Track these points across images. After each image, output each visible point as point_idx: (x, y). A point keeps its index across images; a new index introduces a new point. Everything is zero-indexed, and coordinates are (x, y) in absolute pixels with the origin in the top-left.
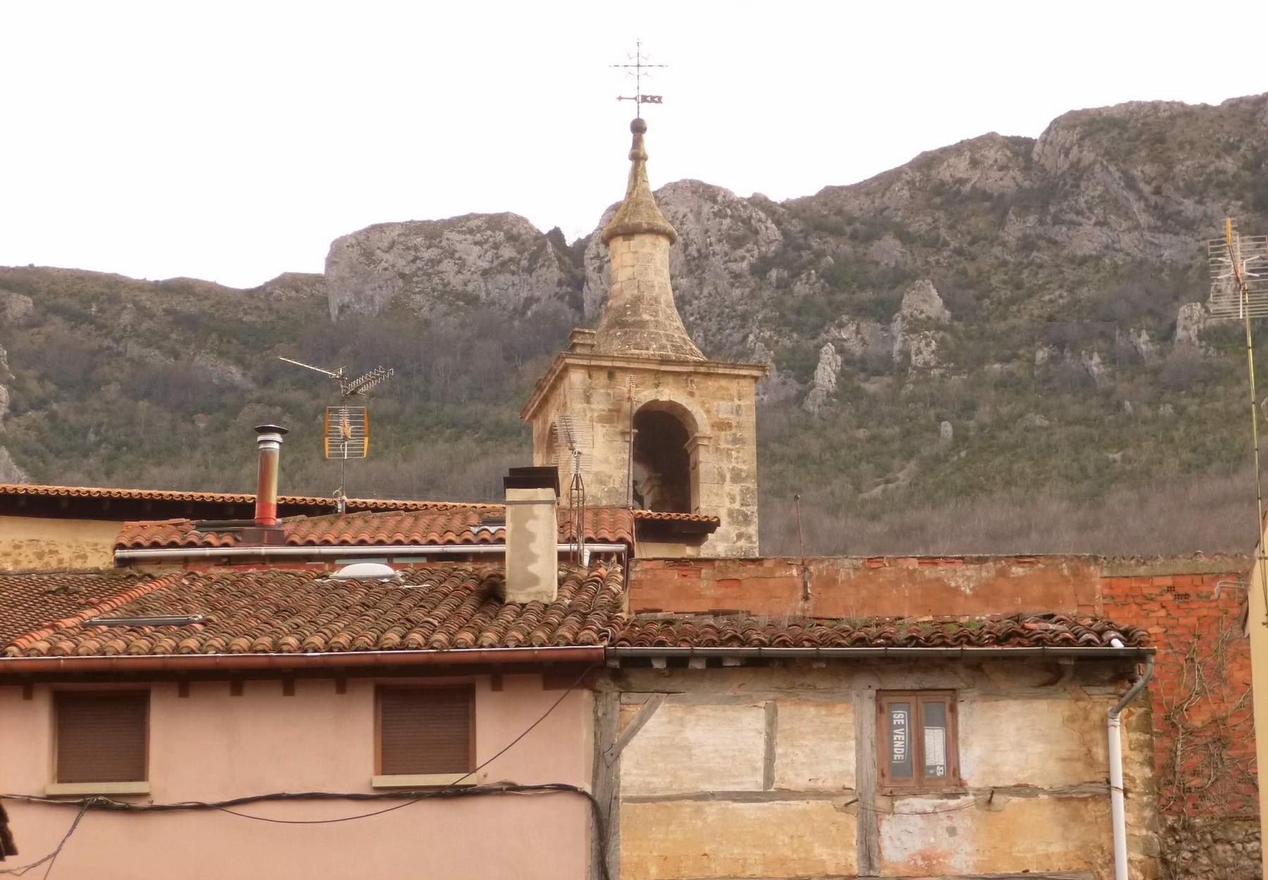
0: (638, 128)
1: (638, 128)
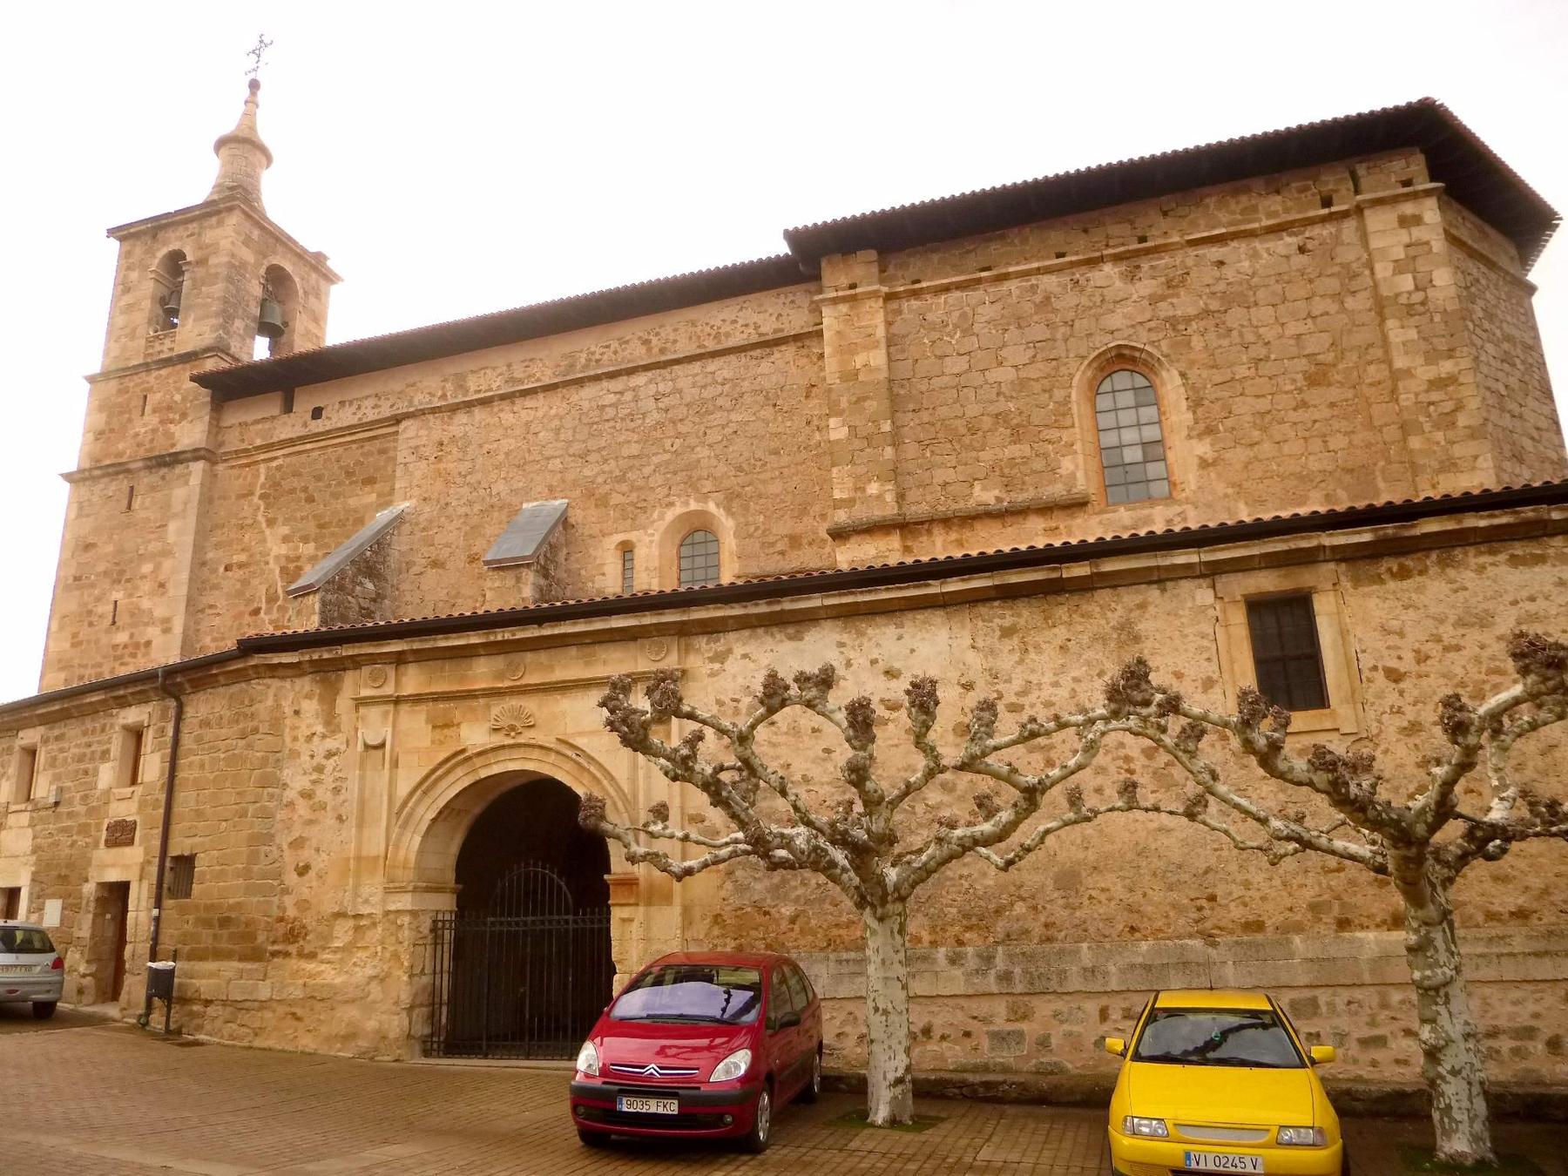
0: (254, 85)
1: (254, 85)
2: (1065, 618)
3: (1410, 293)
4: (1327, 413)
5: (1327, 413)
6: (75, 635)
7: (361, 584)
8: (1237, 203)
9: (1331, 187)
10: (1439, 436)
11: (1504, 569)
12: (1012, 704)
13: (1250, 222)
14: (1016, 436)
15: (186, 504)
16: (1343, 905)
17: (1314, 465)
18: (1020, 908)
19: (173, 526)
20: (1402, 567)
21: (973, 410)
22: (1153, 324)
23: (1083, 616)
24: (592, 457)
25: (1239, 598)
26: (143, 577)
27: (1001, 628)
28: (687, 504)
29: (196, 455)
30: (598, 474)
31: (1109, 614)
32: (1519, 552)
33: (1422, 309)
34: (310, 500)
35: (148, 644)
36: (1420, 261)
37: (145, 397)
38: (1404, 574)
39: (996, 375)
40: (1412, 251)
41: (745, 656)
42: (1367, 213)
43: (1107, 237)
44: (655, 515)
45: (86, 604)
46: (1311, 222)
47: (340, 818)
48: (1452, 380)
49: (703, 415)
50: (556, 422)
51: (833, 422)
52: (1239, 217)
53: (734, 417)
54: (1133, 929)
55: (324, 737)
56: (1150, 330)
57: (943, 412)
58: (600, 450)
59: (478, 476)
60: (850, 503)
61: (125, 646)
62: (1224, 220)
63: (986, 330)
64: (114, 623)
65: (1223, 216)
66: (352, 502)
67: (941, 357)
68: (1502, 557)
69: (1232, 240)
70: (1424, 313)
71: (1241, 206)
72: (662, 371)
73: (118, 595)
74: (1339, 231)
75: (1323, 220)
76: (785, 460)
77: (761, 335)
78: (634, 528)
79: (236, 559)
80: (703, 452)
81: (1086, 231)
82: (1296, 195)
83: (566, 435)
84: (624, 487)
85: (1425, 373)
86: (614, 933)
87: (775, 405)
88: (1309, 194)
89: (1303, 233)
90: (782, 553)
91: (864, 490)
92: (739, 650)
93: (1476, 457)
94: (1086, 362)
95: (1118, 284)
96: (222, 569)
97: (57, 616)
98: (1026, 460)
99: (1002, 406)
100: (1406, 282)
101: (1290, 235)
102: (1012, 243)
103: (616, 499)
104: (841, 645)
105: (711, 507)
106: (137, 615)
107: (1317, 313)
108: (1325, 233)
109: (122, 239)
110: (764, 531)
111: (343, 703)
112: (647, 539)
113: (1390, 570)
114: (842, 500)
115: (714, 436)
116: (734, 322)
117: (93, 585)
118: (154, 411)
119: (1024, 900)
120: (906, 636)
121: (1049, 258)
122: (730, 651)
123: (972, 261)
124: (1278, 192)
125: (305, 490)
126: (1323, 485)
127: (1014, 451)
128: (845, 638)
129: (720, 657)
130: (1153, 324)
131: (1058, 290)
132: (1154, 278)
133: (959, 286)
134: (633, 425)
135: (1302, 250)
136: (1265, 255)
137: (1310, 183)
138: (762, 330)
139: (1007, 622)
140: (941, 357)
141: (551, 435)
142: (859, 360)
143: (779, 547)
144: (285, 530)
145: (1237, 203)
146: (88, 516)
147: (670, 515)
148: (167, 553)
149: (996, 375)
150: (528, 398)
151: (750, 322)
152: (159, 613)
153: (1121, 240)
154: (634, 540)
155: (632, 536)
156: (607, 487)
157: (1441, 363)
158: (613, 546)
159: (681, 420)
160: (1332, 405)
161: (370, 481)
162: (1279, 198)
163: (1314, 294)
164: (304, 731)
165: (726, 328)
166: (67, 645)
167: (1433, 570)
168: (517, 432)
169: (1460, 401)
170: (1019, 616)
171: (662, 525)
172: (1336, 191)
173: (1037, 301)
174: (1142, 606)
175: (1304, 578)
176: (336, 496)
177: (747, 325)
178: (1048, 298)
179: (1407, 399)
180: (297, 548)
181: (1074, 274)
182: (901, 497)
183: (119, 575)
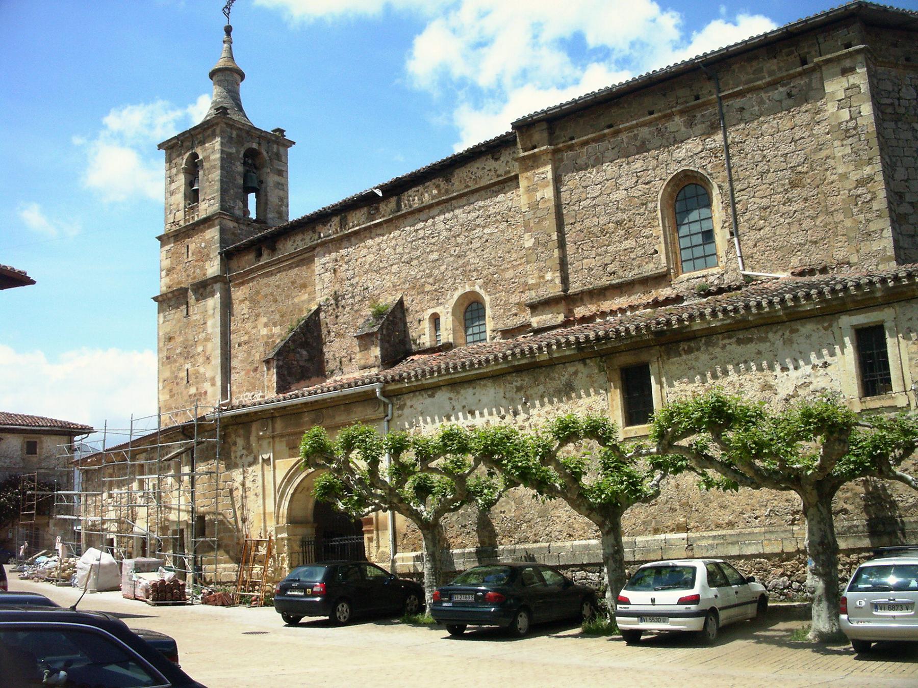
0: (228, 30)
2: (543, 380)
3: (847, 122)
4: (801, 205)
5: (801, 205)
6: (171, 391)
7: (299, 353)
8: (751, 66)
9: (806, 50)
10: (861, 217)
11: (734, 346)
12: (521, 426)
13: (759, 79)
14: (627, 235)
15: (214, 309)
16: (656, 522)
17: (794, 241)
18: (524, 526)
19: (209, 323)
20: (689, 347)
21: (603, 220)
22: (703, 154)
23: (550, 379)
24: (415, 262)
25: (616, 367)
26: (199, 354)
27: (516, 387)
28: (464, 287)
29: (215, 279)
30: (417, 272)
31: (562, 377)
32: (741, 337)
33: (854, 132)
34: (275, 301)
35: (206, 393)
36: (853, 99)
37: (188, 246)
38: (689, 351)
39: (616, 196)
40: (849, 93)
41: (411, 406)
42: (823, 68)
43: (677, 98)
44: (448, 297)
45: (174, 372)
46: (794, 77)
47: (256, 494)
48: (870, 179)
49: (470, 231)
50: (394, 242)
51: (527, 236)
52: (752, 76)
53: (486, 231)
54: (570, 536)
55: (247, 456)
56: (702, 158)
57: (587, 223)
58: (418, 258)
59: (357, 279)
60: (536, 286)
61: (195, 395)
62: (743, 79)
63: (610, 167)
64: (188, 382)
65: (743, 77)
66: (296, 300)
67: (586, 187)
68: (733, 340)
69: (748, 93)
70: (855, 135)
71: (754, 68)
72: (446, 204)
73: (188, 366)
74: (811, 81)
75: (800, 74)
76: (514, 256)
77: (498, 176)
78: (439, 304)
79: (243, 339)
80: (471, 255)
81: (664, 95)
82: (785, 58)
83: (399, 249)
84: (431, 280)
85: (854, 176)
86: (366, 544)
87: (507, 221)
88: (793, 56)
89: (789, 83)
90: (516, 315)
91: (543, 277)
92: (409, 403)
93: (882, 230)
94: (666, 183)
95: (683, 129)
96: (237, 346)
97: (161, 380)
98: (632, 250)
99: (620, 216)
100: (845, 114)
101: (782, 86)
102: (624, 108)
103: (428, 288)
104: (450, 399)
105: (477, 289)
106: (198, 376)
107: (797, 138)
108: (802, 82)
109: (166, 149)
110: (505, 301)
111: (253, 439)
112: (445, 311)
113: (684, 349)
114: (533, 284)
115: (476, 244)
116: (483, 168)
117: (175, 361)
118: (193, 254)
119: (526, 522)
120: (477, 393)
121: (643, 115)
122: (405, 404)
123: (603, 122)
124: (775, 57)
125: (272, 294)
126: (799, 253)
127: (627, 244)
128: (452, 395)
129: (401, 408)
130: (703, 154)
131: (650, 136)
132: (703, 123)
133: (594, 140)
134: (433, 240)
135: (789, 95)
136: (767, 101)
137: (793, 48)
138: (499, 172)
139: (519, 384)
140: (586, 187)
141: (392, 251)
142: (539, 195)
143: (514, 311)
144: (265, 320)
145: (751, 66)
146: (168, 321)
147: (457, 295)
148: (207, 339)
149: (616, 196)
150: (378, 228)
151: (492, 167)
152: (209, 375)
153: (685, 99)
154: (438, 312)
155: (437, 310)
156: (423, 280)
157: (864, 168)
158: (428, 317)
159: (458, 235)
160: (806, 200)
161: (304, 286)
162: (775, 61)
163: (796, 125)
164: (239, 454)
165: (479, 173)
166: (168, 397)
167: (703, 348)
168: (374, 249)
169: (874, 193)
170: (524, 381)
171: (452, 302)
172: (809, 53)
173: (638, 145)
174: (576, 373)
175: (644, 357)
176: (287, 297)
177: (490, 170)
178: (643, 143)
179: (844, 194)
180: (271, 330)
181: (658, 125)
182: (565, 280)
183: (188, 355)
